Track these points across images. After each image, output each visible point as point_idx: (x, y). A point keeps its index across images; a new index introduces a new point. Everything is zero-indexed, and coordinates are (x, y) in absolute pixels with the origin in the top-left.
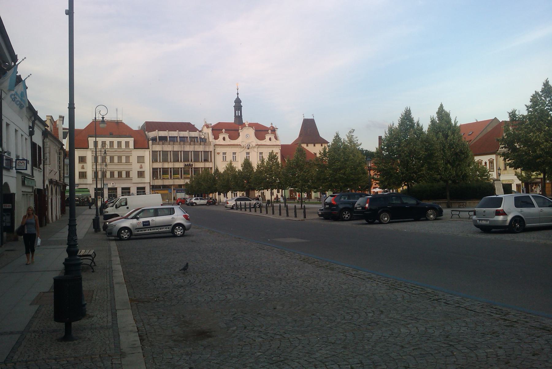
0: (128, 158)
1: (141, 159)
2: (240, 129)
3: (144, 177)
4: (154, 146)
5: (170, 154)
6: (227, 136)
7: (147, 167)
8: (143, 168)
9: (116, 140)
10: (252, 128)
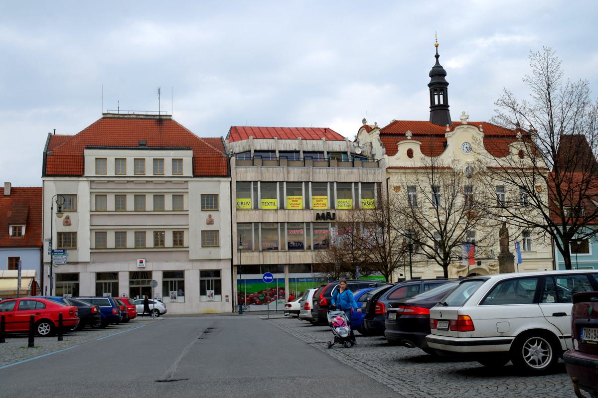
0: (178, 198)
1: (210, 202)
2: (448, 129)
3: (219, 247)
4: (241, 170)
5: (356, 190)
6: (416, 147)
7: (223, 221)
8: (215, 224)
9: (149, 156)
10: (476, 128)
